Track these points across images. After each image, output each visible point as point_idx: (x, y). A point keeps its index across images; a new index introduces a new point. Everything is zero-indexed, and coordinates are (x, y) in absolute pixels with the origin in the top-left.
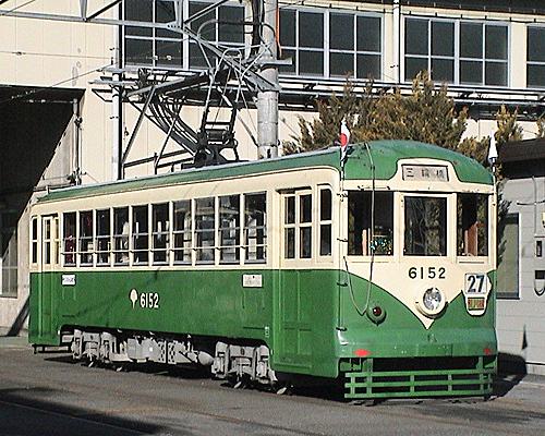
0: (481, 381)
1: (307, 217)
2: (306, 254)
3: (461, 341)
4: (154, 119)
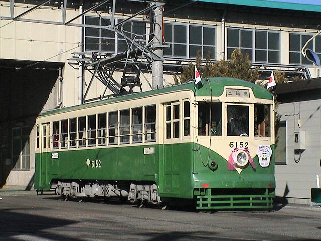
0: (267, 201)
1: (177, 116)
2: (177, 135)
3: (255, 180)
4: (99, 78)
